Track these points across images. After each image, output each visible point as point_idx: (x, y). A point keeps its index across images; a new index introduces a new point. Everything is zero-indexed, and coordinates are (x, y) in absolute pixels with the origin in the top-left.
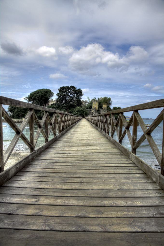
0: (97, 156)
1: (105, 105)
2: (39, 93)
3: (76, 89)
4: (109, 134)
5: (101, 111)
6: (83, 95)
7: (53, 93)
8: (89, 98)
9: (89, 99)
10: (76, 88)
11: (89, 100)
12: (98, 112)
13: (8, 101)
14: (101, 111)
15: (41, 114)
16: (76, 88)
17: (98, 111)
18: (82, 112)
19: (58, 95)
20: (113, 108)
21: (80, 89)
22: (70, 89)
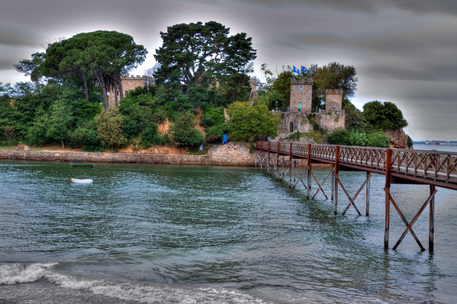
0: (301, 280)
1: (333, 93)
2: (89, 49)
3: (229, 36)
4: (71, 115)
5: (323, 116)
6: (255, 57)
7: (141, 48)
8: (267, 69)
9: (267, 72)
10: (228, 29)
11: (268, 75)
12: (311, 123)
13: (29, 149)
14: (323, 116)
15: (96, 129)
16: (228, 29)
17: (309, 117)
18: (254, 122)
19: (161, 55)
20: (365, 107)
21: (244, 35)
22: (207, 34)
